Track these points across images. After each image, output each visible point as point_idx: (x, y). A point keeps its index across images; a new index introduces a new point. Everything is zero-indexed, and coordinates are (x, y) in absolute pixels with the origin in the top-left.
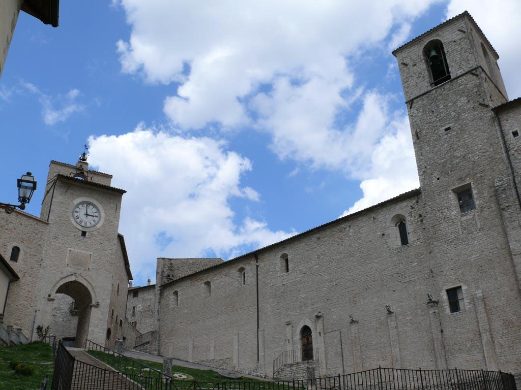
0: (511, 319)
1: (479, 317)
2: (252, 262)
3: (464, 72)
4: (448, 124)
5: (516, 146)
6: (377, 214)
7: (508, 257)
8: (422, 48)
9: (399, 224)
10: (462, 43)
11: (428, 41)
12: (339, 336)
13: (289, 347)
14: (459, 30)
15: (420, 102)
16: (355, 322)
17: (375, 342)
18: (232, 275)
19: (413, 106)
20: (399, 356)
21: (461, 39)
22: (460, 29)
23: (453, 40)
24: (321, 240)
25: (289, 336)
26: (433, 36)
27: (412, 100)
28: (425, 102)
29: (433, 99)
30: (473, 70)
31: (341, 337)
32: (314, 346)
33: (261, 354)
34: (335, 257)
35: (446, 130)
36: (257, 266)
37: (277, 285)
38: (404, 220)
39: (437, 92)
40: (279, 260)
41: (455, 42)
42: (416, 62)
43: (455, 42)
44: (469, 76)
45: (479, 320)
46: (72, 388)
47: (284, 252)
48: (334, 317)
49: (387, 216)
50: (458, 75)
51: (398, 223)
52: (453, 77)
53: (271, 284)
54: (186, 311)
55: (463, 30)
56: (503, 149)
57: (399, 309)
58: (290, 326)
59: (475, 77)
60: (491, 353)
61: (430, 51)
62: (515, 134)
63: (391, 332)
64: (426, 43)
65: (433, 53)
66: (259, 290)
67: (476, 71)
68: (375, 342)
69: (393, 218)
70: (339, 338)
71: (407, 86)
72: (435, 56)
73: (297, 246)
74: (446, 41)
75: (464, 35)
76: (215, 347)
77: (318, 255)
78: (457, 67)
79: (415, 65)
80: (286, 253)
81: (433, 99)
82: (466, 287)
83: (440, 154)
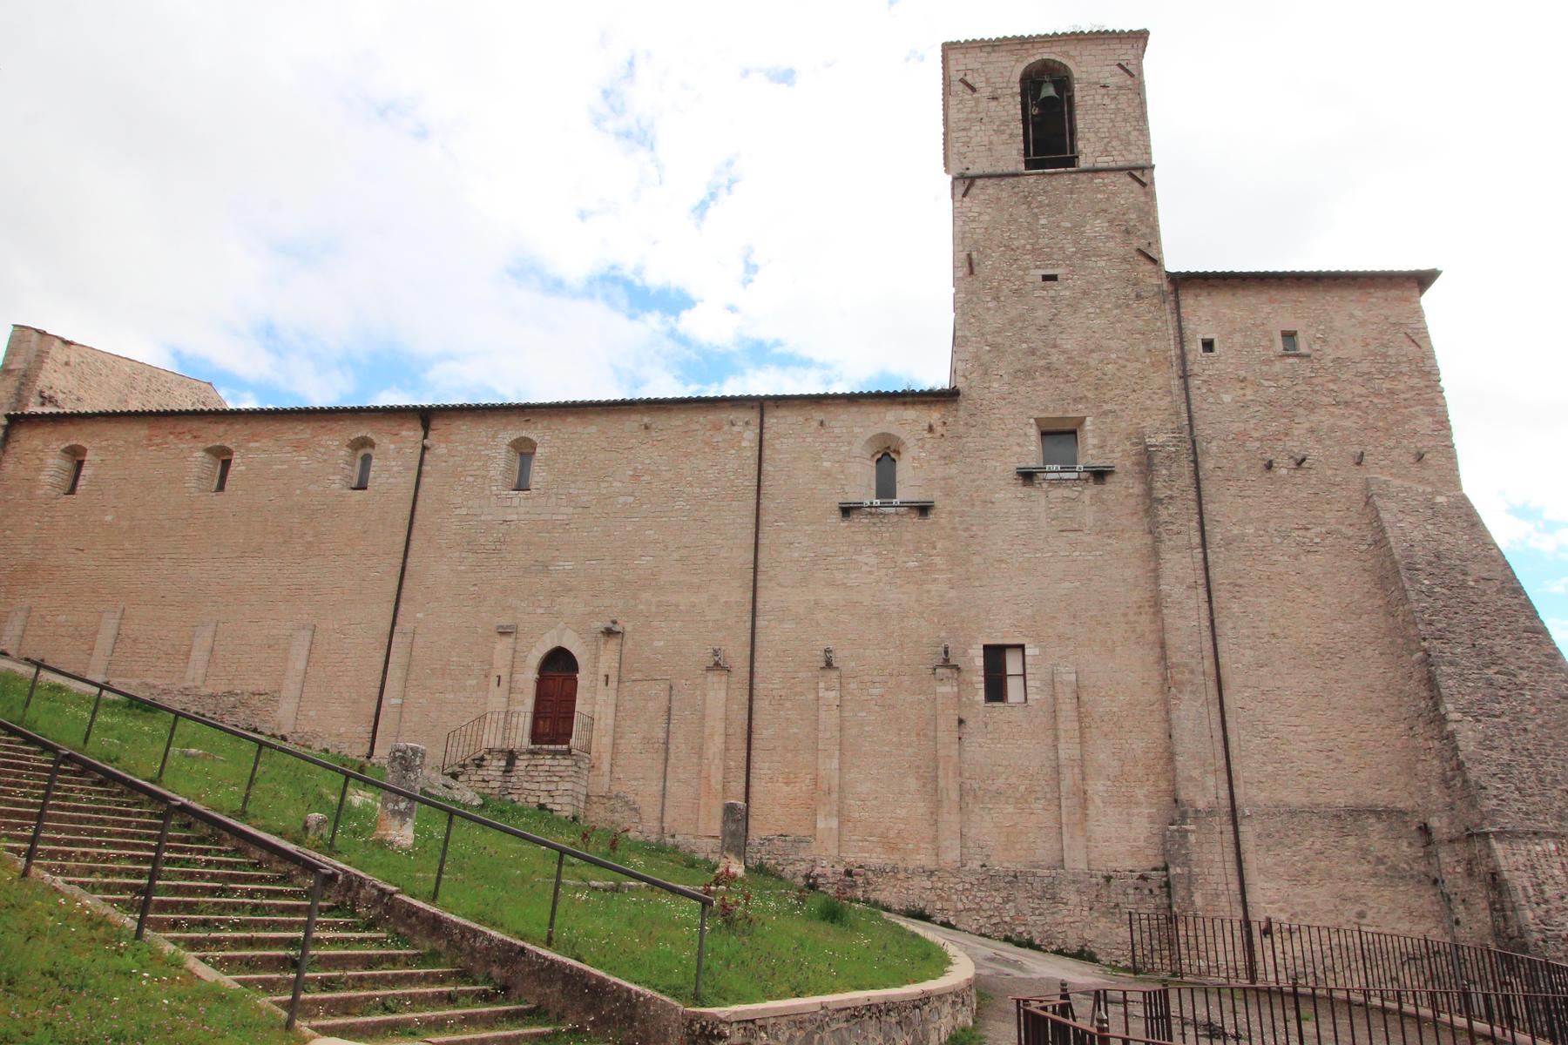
0: (1133, 746)
1: (1061, 727)
2: (404, 433)
3: (1113, 165)
4: (1053, 266)
5: (1207, 372)
6: (832, 415)
7: (1147, 609)
8: (1019, 69)
9: (879, 456)
10: (1123, 99)
11: (1038, 57)
12: (664, 696)
13: (496, 700)
14: (1120, 66)
15: (990, 191)
16: (723, 668)
17: (771, 732)
18: (323, 450)
19: (970, 192)
20: (835, 782)
21: (1119, 88)
22: (1124, 63)
23: (1102, 82)
24: (654, 434)
25: (501, 667)
26: (1054, 49)
27: (973, 179)
28: (1004, 194)
29: (1026, 197)
30: (1136, 169)
31: (670, 701)
32: (581, 706)
33: (392, 700)
34: (687, 490)
35: (1046, 278)
36: (425, 448)
37: (483, 518)
38: (898, 452)
39: (1031, 181)
40: (503, 452)
41: (1104, 86)
42: (999, 91)
43: (1104, 86)
44: (1124, 179)
45: (1062, 734)
46: (816, 1042)
47: (524, 434)
48: (656, 644)
49: (856, 430)
50: (1099, 165)
51: (878, 452)
52: (1083, 163)
53: (464, 511)
54: (109, 518)
55: (1129, 68)
56: (1174, 368)
57: (853, 664)
58: (509, 640)
59: (1137, 185)
60: (1078, 816)
61: (1038, 86)
62: (1208, 345)
63: (822, 715)
64: (1032, 60)
65: (1049, 91)
66: (418, 516)
67: (1143, 175)
68: (771, 732)
69: (871, 440)
70: (665, 703)
71: (964, 139)
72: (1049, 98)
73: (570, 430)
74: (1084, 75)
75: (1129, 82)
76: (212, 650)
77: (635, 469)
78: (1100, 146)
79: (995, 99)
80: (533, 437)
81: (1026, 197)
82: (1036, 651)
83: (1021, 328)
